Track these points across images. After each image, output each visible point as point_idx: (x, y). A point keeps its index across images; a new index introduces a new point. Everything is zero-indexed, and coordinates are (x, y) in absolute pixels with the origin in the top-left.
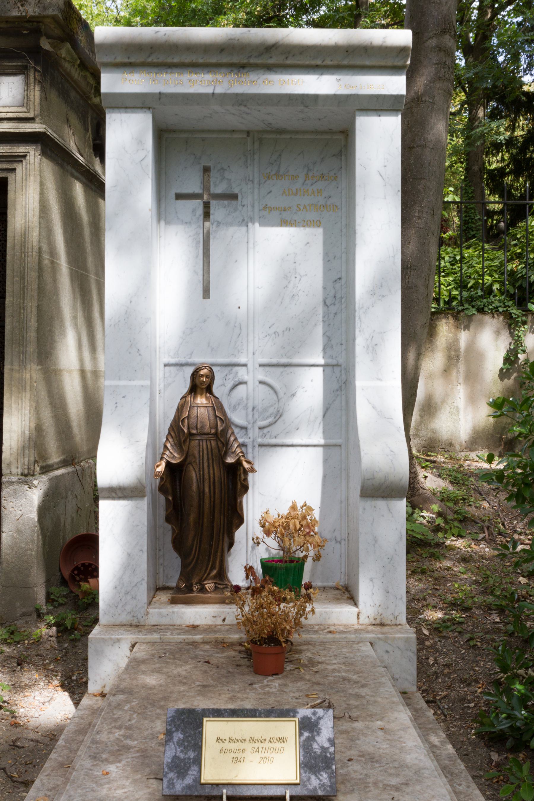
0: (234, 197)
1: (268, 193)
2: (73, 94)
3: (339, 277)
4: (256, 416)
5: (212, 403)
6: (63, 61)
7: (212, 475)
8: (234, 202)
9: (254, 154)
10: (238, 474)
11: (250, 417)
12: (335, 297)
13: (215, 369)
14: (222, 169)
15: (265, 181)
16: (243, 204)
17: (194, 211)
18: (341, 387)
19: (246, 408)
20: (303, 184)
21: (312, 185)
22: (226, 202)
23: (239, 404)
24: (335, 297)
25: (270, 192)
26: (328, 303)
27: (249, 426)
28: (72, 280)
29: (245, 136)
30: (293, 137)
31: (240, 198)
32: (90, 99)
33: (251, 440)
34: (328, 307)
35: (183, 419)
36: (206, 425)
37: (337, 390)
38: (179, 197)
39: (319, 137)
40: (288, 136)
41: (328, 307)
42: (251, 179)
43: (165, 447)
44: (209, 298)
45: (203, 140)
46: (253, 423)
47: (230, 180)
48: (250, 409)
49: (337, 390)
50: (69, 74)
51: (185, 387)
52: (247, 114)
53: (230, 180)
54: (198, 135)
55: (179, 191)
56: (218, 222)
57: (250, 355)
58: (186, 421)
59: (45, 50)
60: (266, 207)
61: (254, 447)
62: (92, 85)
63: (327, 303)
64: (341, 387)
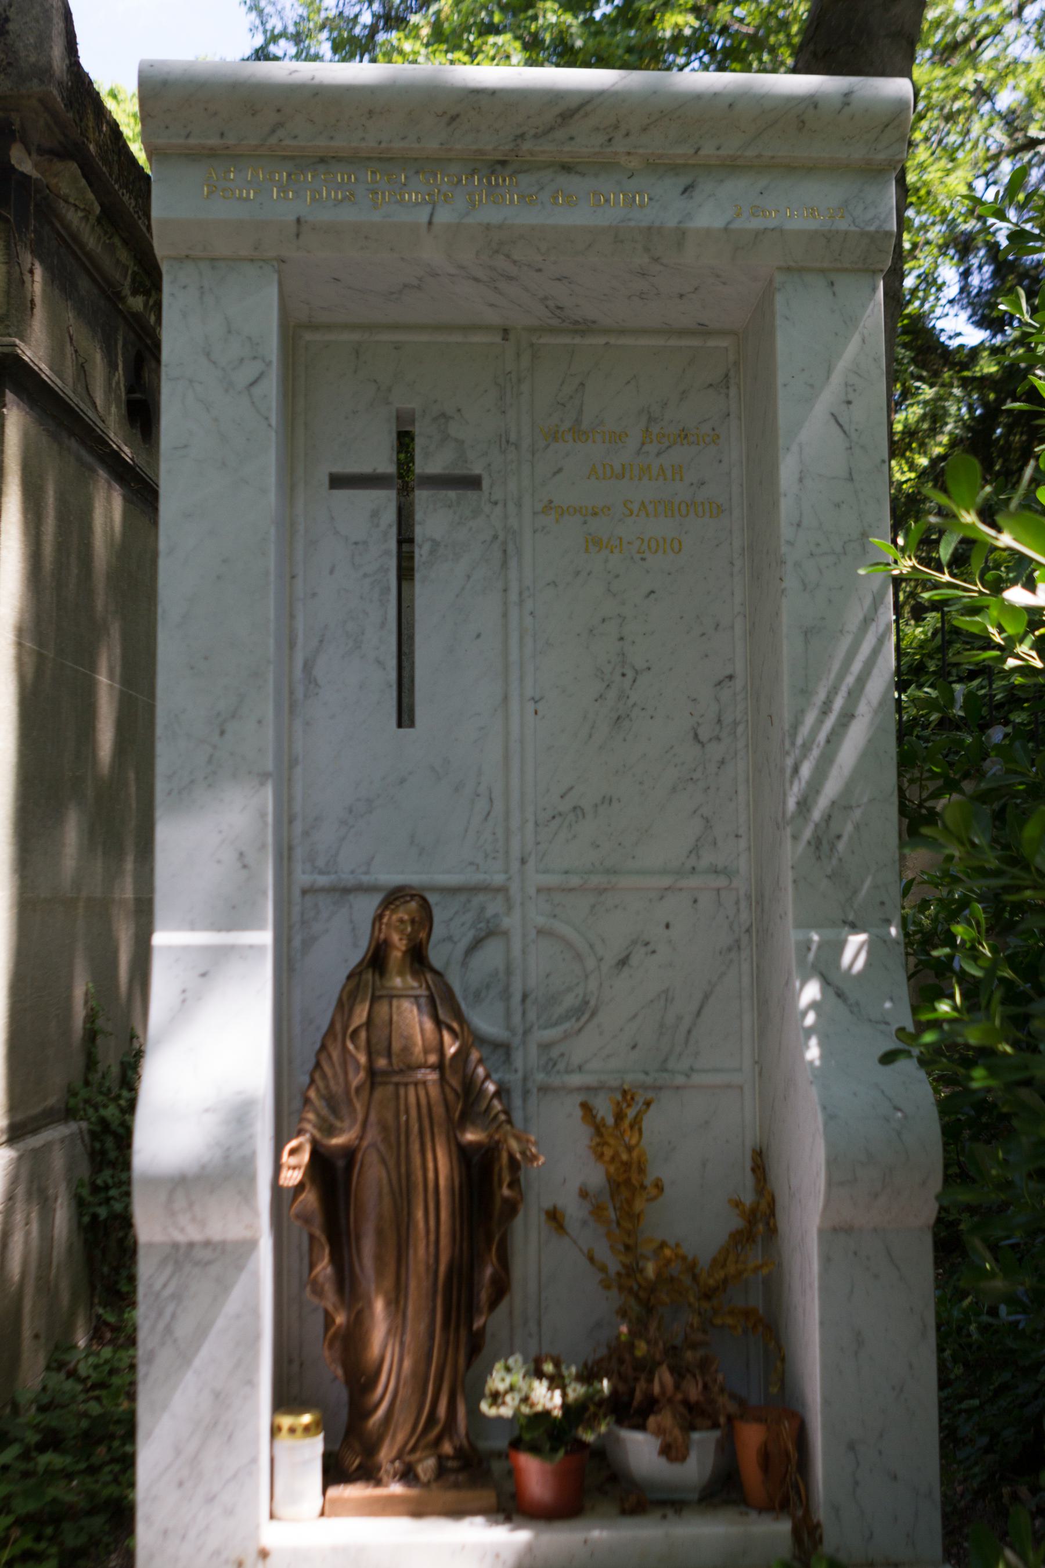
0: (473, 483)
1: (555, 474)
2: (84, 284)
3: (728, 672)
4: (532, 1015)
5: (428, 988)
6: (62, 204)
7: (431, 1175)
8: (471, 495)
9: (519, 381)
10: (496, 1169)
11: (517, 1019)
12: (719, 721)
13: (432, 899)
14: (443, 415)
15: (548, 446)
16: (494, 498)
17: (375, 514)
18: (738, 941)
19: (506, 994)
20: (638, 452)
21: (658, 454)
22: (452, 494)
23: (488, 986)
24: (719, 721)
25: (560, 470)
26: (704, 736)
27: (516, 1041)
28: (43, 302)
29: (498, 339)
30: (613, 341)
31: (485, 484)
32: (123, 299)
33: (520, 1075)
34: (703, 745)
35: (356, 1032)
36: (415, 1044)
37: (730, 949)
38: (338, 481)
39: (673, 342)
40: (601, 340)
41: (703, 745)
42: (513, 437)
43: (307, 1101)
44: (412, 724)
45: (398, 347)
46: (526, 1033)
47: (463, 442)
48: (517, 998)
49: (730, 949)
50: (75, 238)
51: (355, 945)
52: (510, 278)
53: (463, 442)
54: (385, 337)
55: (339, 468)
56: (433, 541)
57: (515, 865)
58: (363, 1035)
59: (22, 174)
60: (549, 507)
61: (526, 1093)
62: (126, 268)
63: (700, 737)
64: (738, 941)
